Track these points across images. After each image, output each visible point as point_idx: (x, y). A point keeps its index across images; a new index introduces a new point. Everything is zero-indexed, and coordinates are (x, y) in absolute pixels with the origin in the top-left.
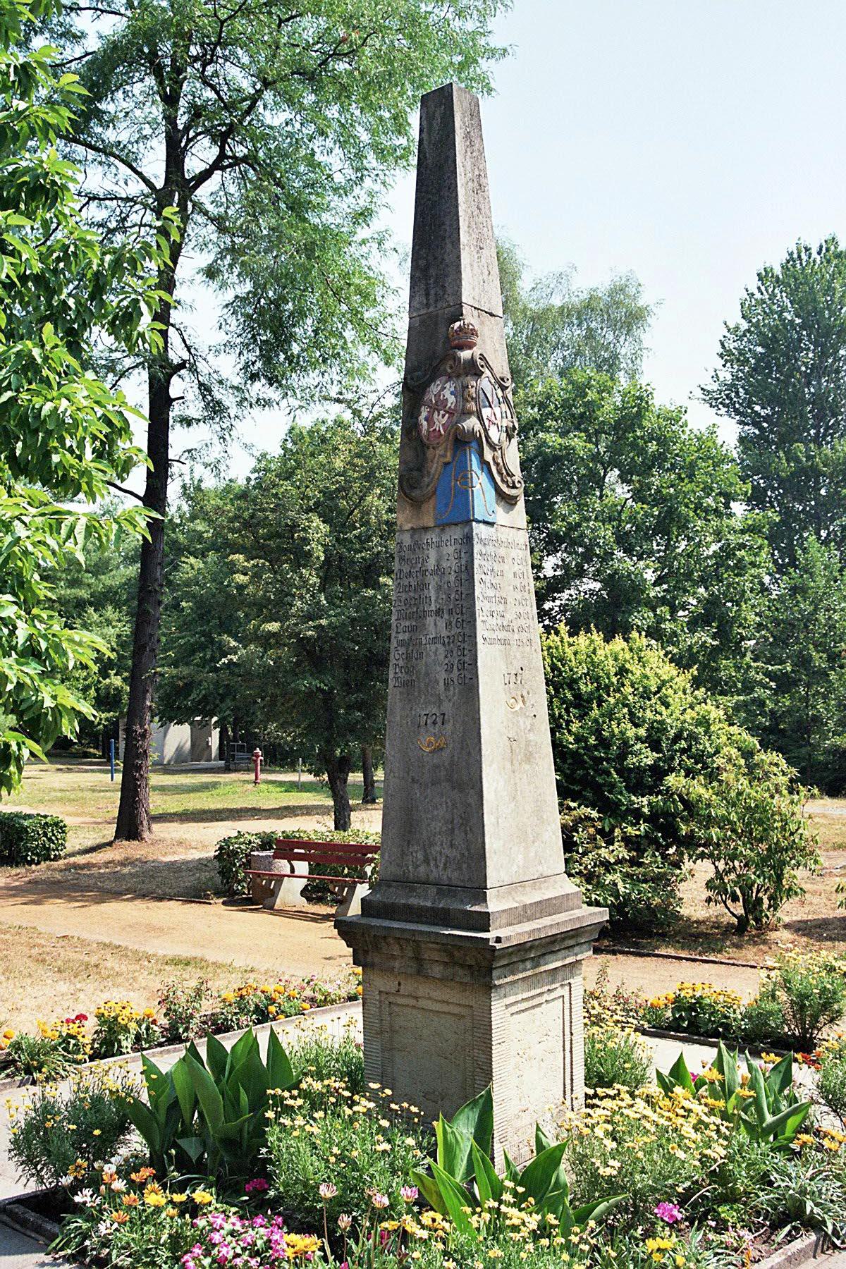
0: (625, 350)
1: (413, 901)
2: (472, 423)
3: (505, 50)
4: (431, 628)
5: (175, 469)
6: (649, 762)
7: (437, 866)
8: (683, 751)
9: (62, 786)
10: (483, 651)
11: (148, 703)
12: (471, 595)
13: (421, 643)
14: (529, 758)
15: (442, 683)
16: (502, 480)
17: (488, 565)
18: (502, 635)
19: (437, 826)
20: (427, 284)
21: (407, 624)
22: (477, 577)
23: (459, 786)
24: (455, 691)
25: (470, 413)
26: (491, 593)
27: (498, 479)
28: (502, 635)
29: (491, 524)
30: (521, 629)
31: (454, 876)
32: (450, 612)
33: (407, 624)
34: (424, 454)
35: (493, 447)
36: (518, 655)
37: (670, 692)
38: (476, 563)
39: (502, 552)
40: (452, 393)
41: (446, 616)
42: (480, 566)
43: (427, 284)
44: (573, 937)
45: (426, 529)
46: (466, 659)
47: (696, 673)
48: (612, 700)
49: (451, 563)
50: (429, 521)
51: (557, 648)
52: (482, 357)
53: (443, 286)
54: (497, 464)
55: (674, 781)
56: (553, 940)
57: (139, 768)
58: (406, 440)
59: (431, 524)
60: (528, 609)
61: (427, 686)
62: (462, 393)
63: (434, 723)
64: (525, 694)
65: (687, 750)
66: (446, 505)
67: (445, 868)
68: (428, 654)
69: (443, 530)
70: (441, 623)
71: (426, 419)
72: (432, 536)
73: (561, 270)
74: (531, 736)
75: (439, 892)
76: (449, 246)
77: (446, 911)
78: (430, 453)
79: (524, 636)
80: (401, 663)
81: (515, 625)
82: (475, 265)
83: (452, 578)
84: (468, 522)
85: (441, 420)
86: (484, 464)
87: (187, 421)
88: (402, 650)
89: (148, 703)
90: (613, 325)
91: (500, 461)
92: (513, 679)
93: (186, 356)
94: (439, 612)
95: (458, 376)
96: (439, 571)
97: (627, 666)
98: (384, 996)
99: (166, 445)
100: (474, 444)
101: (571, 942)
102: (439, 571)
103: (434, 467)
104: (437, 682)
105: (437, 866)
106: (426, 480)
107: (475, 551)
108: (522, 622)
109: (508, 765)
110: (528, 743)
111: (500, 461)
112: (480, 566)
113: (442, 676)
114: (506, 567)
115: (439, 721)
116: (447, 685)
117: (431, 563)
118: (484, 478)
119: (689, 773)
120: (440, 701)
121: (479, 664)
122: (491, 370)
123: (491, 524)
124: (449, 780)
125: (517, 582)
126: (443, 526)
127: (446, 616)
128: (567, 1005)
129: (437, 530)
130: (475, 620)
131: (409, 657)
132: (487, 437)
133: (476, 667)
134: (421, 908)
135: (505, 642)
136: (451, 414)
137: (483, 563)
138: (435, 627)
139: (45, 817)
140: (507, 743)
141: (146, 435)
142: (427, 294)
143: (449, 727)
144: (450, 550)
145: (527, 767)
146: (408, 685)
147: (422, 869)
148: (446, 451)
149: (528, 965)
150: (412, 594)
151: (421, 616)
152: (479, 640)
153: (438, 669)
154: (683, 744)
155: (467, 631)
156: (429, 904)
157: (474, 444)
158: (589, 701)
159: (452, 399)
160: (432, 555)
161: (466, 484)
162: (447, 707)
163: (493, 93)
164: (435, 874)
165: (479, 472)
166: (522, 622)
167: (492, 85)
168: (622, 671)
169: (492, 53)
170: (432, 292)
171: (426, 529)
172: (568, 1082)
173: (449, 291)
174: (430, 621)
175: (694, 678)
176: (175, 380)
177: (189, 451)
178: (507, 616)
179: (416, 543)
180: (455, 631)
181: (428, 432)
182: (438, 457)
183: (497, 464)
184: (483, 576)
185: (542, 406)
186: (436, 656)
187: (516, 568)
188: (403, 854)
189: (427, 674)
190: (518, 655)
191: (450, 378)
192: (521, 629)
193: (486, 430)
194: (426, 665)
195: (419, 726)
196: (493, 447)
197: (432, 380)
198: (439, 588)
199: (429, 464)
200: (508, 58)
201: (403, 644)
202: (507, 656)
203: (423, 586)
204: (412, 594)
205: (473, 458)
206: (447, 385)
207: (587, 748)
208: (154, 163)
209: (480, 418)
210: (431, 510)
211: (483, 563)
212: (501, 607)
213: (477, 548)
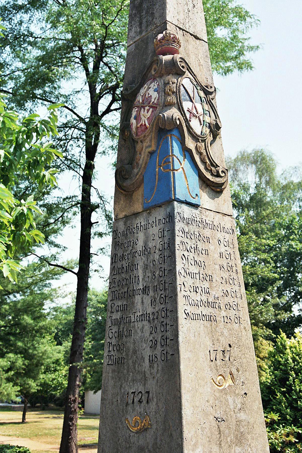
2: (173, 112)
3: (258, 47)
4: (139, 306)
5: (94, 259)
9: (51, 426)
10: (184, 326)
11: (78, 383)
12: (172, 271)
13: (130, 322)
14: (240, 439)
15: (147, 361)
16: (206, 169)
17: (190, 243)
18: (207, 311)
21: (120, 303)
22: (178, 254)
24: (159, 366)
25: (170, 105)
26: (194, 269)
27: (202, 167)
28: (207, 311)
29: (196, 206)
30: (228, 306)
32: (155, 290)
33: (120, 303)
34: (135, 148)
35: (195, 137)
36: (226, 332)
38: (178, 240)
39: (207, 232)
41: (151, 293)
42: (182, 242)
43: (141, 16)
45: (136, 215)
46: (169, 334)
49: (156, 243)
50: (138, 207)
51: (295, 347)
53: (153, 13)
54: (200, 154)
57: (72, 419)
58: (123, 142)
59: (140, 210)
60: (236, 288)
61: (134, 363)
62: (164, 91)
63: (140, 402)
64: (234, 371)
66: (152, 189)
68: (136, 331)
69: (149, 213)
70: (147, 300)
71: (136, 118)
72: (141, 221)
73: (296, 165)
74: (242, 416)
78: (138, 146)
79: (232, 313)
80: (114, 341)
81: (223, 302)
83: (157, 257)
84: (170, 202)
85: (146, 115)
86: (186, 151)
87: (100, 235)
88: (115, 329)
89: (78, 383)
91: (203, 151)
92: (220, 356)
93: (99, 201)
94: (145, 290)
95: (161, 76)
96: (146, 251)
99: (89, 247)
100: (175, 132)
102: (146, 251)
103: (142, 158)
106: (136, 171)
107: (177, 228)
108: (229, 300)
110: (239, 422)
111: (203, 151)
112: (182, 242)
113: (147, 352)
114: (211, 247)
116: (151, 362)
118: (186, 164)
120: (145, 379)
121: (181, 339)
123: (196, 206)
125: (224, 262)
126: (149, 210)
127: (151, 293)
129: (145, 214)
130: (176, 295)
131: (120, 336)
132: (189, 128)
133: (177, 342)
135: (210, 319)
136: (154, 107)
137: (185, 240)
138: (143, 304)
139: (20, 447)
140: (214, 423)
141: (79, 241)
142: (141, 24)
143: (153, 406)
144: (155, 230)
148: (151, 141)
150: (123, 275)
152: (181, 315)
153: (145, 345)
155: (169, 307)
157: (175, 132)
160: (141, 236)
161: (168, 167)
162: (152, 385)
163: (253, 69)
165: (181, 158)
166: (229, 300)
167: (253, 65)
169: (251, 48)
171: (136, 215)
173: (157, 15)
174: (138, 299)
176: (93, 214)
177: (101, 249)
178: (213, 293)
179: (128, 228)
181: (137, 128)
182: (147, 146)
183: (200, 154)
184: (186, 253)
185: (288, 228)
189: (135, 352)
190: (226, 332)
191: (154, 79)
192: (228, 306)
193: (187, 121)
194: (134, 343)
195: (127, 404)
196: (195, 137)
197: (141, 86)
198: (146, 267)
199: (138, 156)
200: (260, 50)
202: (212, 333)
203: (132, 266)
204: (123, 275)
205: (175, 144)
206: (152, 85)
208: (84, 111)
209: (181, 109)
210: (140, 197)
211: (185, 240)
212: (206, 285)
213: (178, 226)
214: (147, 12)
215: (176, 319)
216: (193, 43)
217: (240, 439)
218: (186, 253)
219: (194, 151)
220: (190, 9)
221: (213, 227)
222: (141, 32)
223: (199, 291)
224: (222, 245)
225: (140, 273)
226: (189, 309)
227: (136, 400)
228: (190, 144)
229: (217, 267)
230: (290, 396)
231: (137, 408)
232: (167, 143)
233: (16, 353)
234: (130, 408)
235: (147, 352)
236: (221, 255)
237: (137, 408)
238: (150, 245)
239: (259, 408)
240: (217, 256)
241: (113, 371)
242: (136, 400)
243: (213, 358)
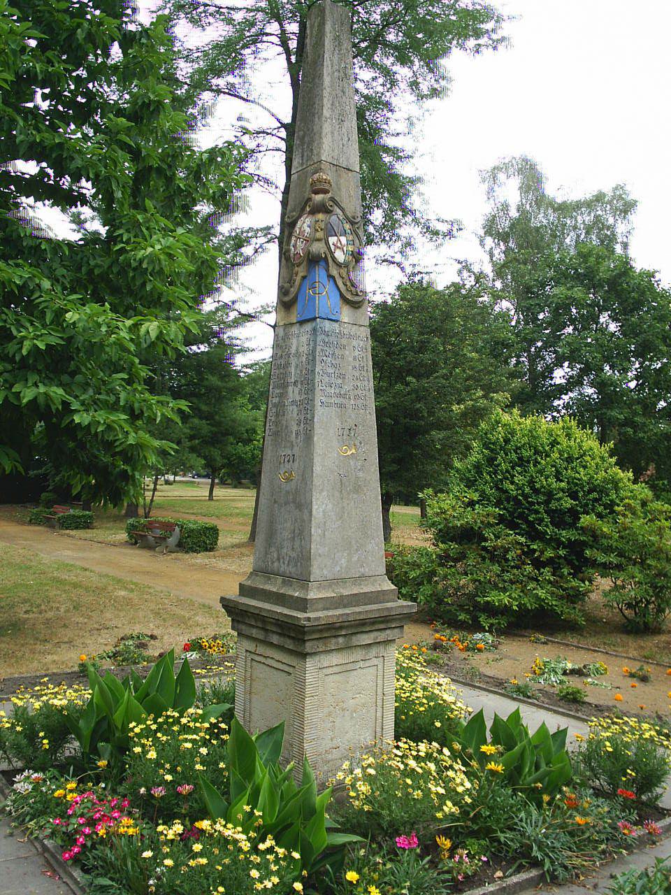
0: (621, 228)
1: (267, 587)
4: (290, 394)
6: (569, 506)
7: (284, 563)
8: (596, 500)
19: (286, 534)
20: (303, 149)
23: (300, 506)
24: (301, 437)
30: (357, 397)
31: (291, 570)
33: (278, 391)
35: (339, 265)
37: (588, 458)
39: (344, 341)
40: (309, 226)
41: (299, 386)
43: (303, 149)
44: (382, 622)
45: (292, 324)
47: (612, 446)
48: (543, 462)
49: (304, 349)
52: (332, 199)
53: (312, 150)
55: (586, 520)
56: (363, 623)
60: (366, 383)
61: (286, 435)
63: (289, 461)
65: (599, 497)
67: (288, 565)
70: (297, 391)
72: (295, 329)
74: (361, 474)
75: (284, 582)
76: (317, 119)
77: (283, 595)
79: (360, 402)
80: (273, 419)
82: (336, 134)
83: (304, 359)
90: (615, 211)
92: (346, 432)
97: (559, 440)
98: (248, 654)
101: (382, 626)
102: (298, 354)
104: (292, 432)
105: (284, 563)
109: (337, 494)
115: (291, 460)
116: (297, 434)
117: (293, 350)
119: (600, 516)
122: (343, 210)
124: (294, 502)
126: (302, 323)
128: (380, 673)
131: (277, 415)
132: (334, 259)
134: (270, 592)
135: (341, 406)
140: (338, 477)
142: (302, 156)
143: (296, 464)
144: (304, 339)
145: (355, 496)
146: (276, 434)
147: (276, 564)
149: (341, 640)
150: (281, 371)
151: (284, 386)
152: (318, 403)
154: (595, 495)
156: (274, 590)
158: (528, 462)
159: (308, 230)
160: (294, 341)
162: (296, 450)
164: (282, 569)
168: (554, 443)
170: (305, 154)
171: (292, 324)
172: (379, 730)
173: (315, 152)
174: (290, 389)
175: (611, 450)
180: (304, 396)
181: (294, 255)
184: (325, 358)
186: (292, 413)
187: (357, 353)
188: (266, 553)
189: (287, 427)
192: (357, 397)
193: (332, 253)
198: (297, 366)
201: (275, 405)
203: (287, 365)
204: (281, 371)
207: (523, 494)
214: (308, 147)
215: (314, 406)
216: (345, 176)
217: (357, 489)
218: (325, 358)
219: (337, 277)
220: (345, 143)
221: (350, 337)
222: (302, 164)
223: (333, 386)
224: (356, 350)
225: (293, 370)
226: (324, 399)
227: (286, 460)
228: (334, 272)
229: (350, 368)
230: (496, 477)
231: (287, 466)
232: (315, 272)
233: (201, 418)
234: (282, 466)
235: (295, 428)
236: (355, 359)
237: (287, 466)
238: (301, 350)
239: (375, 470)
240: (351, 359)
241: (272, 440)
242: (286, 460)
243: (340, 433)
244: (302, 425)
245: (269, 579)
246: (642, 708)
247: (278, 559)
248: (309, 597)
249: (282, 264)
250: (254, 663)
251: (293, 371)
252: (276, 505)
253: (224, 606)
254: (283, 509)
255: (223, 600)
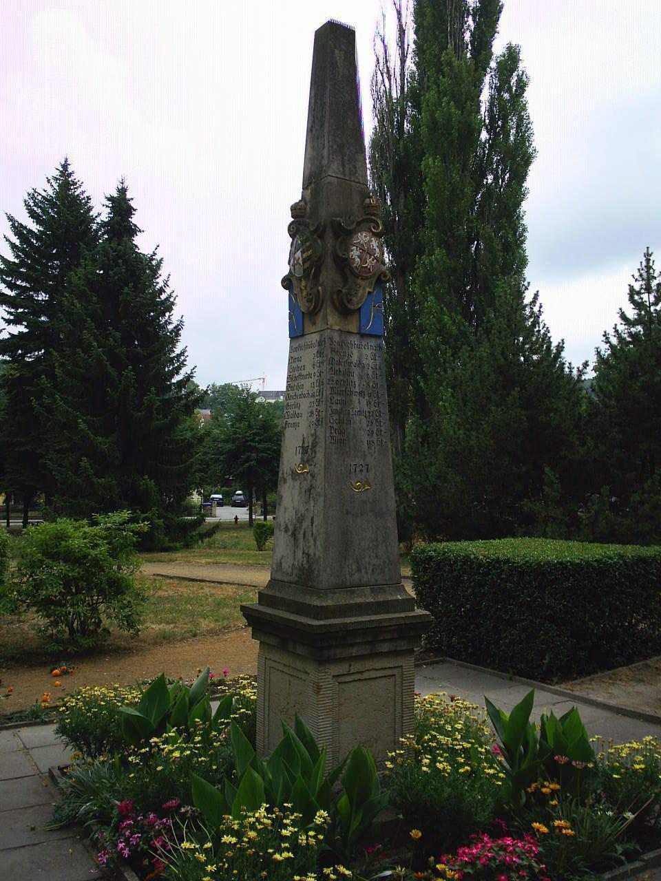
63: (361, 471)
70: (364, 402)
83: (370, 373)
105: (367, 573)
143: (372, 474)
171: (350, 333)
231: (359, 475)
234: (352, 475)
241: (336, 449)
242: (358, 470)
244: (375, 435)
245: (353, 592)
246: (33, 829)
247: (359, 571)
248: (328, 317)
249: (307, 152)
250: (272, 670)
251: (356, 379)
252: (350, 516)
253: (244, 615)
254: (359, 520)
255: (243, 608)
